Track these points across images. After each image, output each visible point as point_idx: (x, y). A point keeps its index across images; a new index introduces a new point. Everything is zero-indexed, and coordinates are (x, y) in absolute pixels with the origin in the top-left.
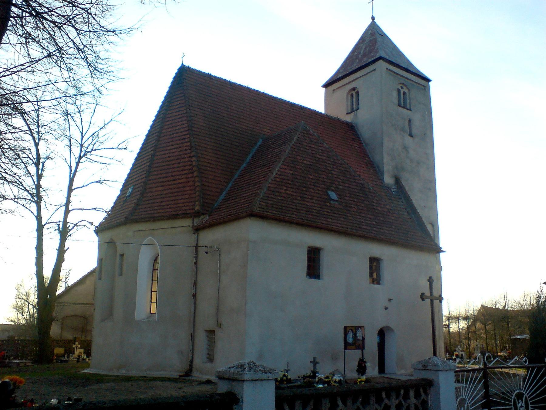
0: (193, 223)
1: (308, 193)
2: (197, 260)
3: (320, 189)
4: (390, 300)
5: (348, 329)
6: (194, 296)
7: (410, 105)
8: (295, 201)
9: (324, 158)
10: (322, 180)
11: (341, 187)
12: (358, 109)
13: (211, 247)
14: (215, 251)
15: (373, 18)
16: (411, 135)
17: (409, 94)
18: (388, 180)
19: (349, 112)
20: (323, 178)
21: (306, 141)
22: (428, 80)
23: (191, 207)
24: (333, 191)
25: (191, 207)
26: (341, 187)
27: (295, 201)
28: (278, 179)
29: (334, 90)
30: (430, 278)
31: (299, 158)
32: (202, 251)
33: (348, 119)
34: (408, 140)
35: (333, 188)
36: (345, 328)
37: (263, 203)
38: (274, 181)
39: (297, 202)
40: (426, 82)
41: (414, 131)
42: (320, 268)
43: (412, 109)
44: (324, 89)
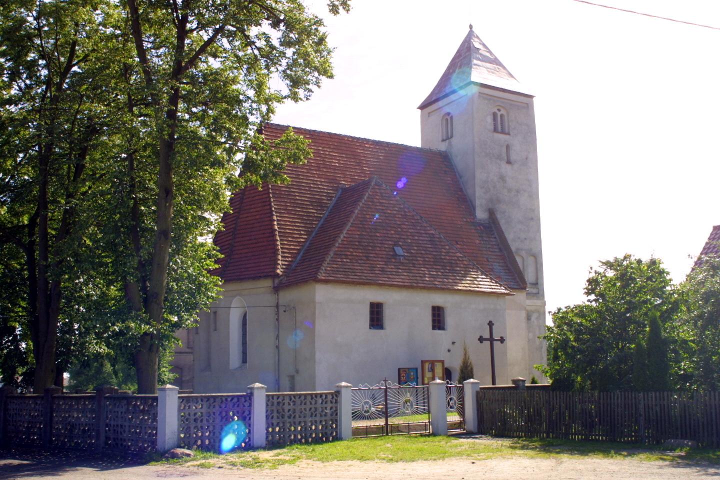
0: (274, 282)
1: (373, 252)
2: (278, 316)
3: (386, 246)
4: (453, 343)
5: (401, 370)
6: (277, 347)
7: (509, 129)
8: (360, 262)
9: (395, 212)
10: (390, 236)
11: (409, 241)
12: (452, 137)
13: (288, 306)
14: (291, 309)
15: (471, 27)
16: (509, 162)
17: (508, 116)
18: (481, 214)
19: (445, 138)
20: (392, 234)
21: (378, 197)
22: (531, 97)
23: (272, 270)
24: (400, 246)
25: (272, 270)
26: (409, 241)
27: (360, 262)
28: (345, 243)
29: (429, 113)
30: (490, 322)
31: (368, 216)
32: (281, 310)
33: (443, 147)
34: (506, 169)
35: (400, 243)
36: (399, 369)
37: (328, 269)
38: (342, 244)
39: (362, 261)
40: (529, 99)
41: (513, 157)
42: (382, 319)
43: (511, 133)
44: (420, 111)
